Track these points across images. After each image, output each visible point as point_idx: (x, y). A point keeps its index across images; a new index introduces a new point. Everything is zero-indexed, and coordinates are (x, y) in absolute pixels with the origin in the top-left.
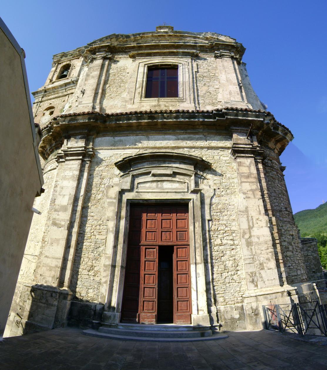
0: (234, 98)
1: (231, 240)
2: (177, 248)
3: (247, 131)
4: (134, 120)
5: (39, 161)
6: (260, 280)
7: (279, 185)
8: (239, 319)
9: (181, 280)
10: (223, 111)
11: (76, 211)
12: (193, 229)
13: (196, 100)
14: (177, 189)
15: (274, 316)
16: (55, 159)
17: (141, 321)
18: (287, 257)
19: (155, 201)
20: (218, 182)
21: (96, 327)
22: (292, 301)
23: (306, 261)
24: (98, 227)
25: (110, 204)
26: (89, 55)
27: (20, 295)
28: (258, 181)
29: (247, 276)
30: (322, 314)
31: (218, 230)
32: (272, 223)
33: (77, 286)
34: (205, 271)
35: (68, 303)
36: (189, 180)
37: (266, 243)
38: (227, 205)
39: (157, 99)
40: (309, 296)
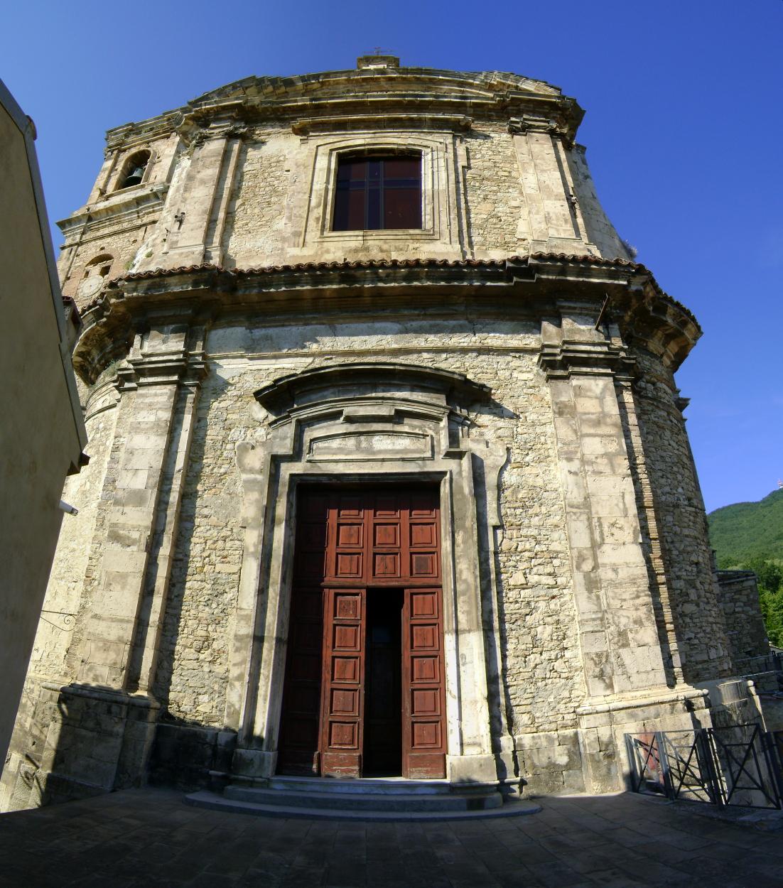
0: (558, 230)
1: (549, 574)
2: (412, 594)
3: (595, 310)
4: (307, 284)
5: (75, 388)
6: (620, 671)
7: (674, 444)
8: (568, 767)
9: (421, 670)
10: (530, 261)
11: (167, 503)
12: (449, 549)
13: (465, 235)
14: (405, 451)
15: (652, 759)
16: (114, 382)
17: (325, 771)
18: (686, 616)
19: (357, 477)
20: (507, 433)
21: (216, 787)
22: (696, 723)
23: (728, 627)
24: (220, 543)
25: (249, 485)
26: (193, 129)
27: (33, 709)
28: (622, 433)
29: (588, 661)
30: (768, 755)
31: (519, 549)
32: (648, 534)
33: (171, 688)
34: (485, 650)
35: (150, 728)
36: (434, 431)
37: (633, 581)
38: (539, 490)
39: (361, 233)
40: (738, 712)
